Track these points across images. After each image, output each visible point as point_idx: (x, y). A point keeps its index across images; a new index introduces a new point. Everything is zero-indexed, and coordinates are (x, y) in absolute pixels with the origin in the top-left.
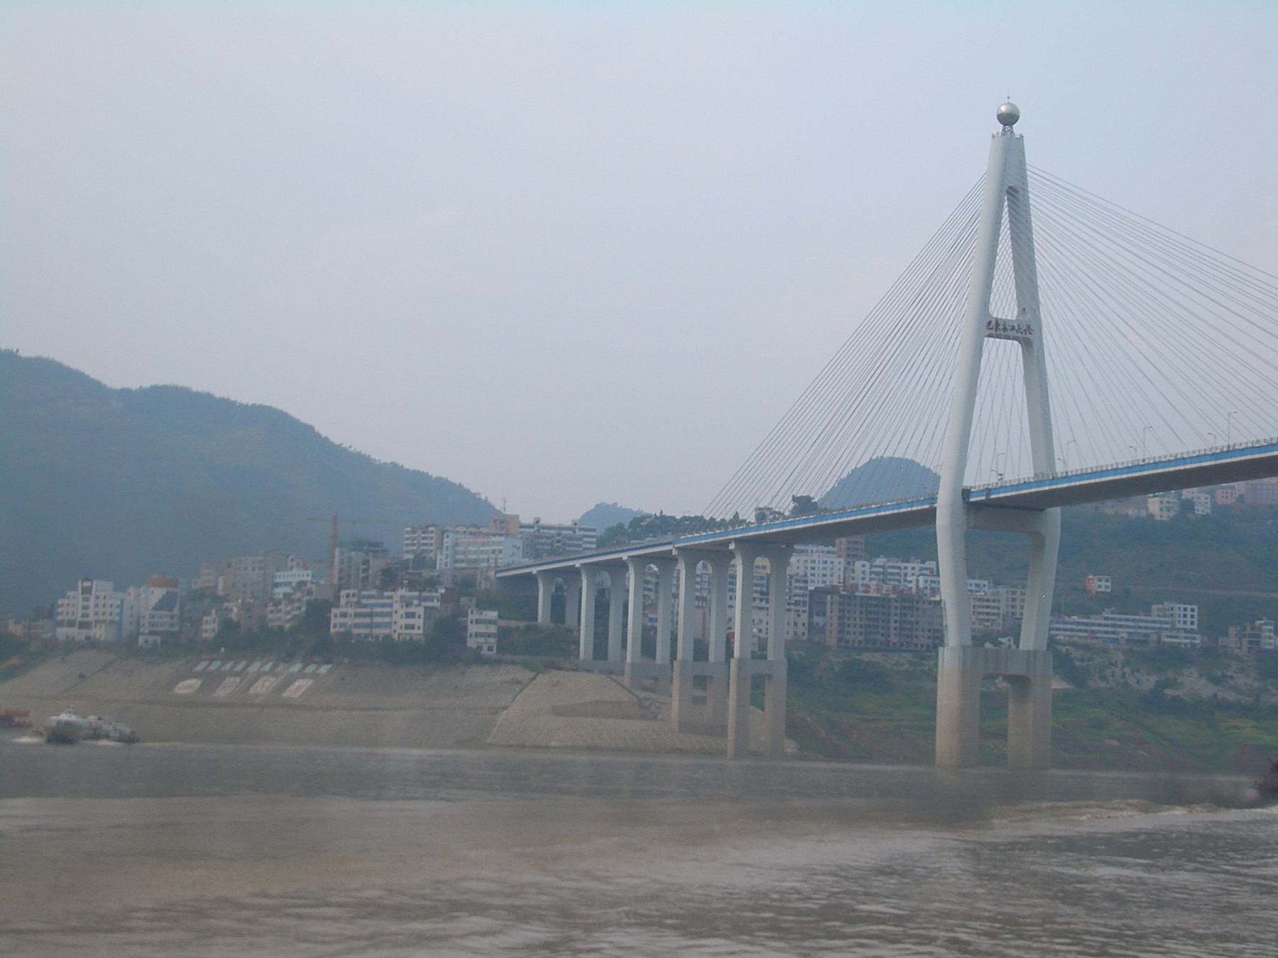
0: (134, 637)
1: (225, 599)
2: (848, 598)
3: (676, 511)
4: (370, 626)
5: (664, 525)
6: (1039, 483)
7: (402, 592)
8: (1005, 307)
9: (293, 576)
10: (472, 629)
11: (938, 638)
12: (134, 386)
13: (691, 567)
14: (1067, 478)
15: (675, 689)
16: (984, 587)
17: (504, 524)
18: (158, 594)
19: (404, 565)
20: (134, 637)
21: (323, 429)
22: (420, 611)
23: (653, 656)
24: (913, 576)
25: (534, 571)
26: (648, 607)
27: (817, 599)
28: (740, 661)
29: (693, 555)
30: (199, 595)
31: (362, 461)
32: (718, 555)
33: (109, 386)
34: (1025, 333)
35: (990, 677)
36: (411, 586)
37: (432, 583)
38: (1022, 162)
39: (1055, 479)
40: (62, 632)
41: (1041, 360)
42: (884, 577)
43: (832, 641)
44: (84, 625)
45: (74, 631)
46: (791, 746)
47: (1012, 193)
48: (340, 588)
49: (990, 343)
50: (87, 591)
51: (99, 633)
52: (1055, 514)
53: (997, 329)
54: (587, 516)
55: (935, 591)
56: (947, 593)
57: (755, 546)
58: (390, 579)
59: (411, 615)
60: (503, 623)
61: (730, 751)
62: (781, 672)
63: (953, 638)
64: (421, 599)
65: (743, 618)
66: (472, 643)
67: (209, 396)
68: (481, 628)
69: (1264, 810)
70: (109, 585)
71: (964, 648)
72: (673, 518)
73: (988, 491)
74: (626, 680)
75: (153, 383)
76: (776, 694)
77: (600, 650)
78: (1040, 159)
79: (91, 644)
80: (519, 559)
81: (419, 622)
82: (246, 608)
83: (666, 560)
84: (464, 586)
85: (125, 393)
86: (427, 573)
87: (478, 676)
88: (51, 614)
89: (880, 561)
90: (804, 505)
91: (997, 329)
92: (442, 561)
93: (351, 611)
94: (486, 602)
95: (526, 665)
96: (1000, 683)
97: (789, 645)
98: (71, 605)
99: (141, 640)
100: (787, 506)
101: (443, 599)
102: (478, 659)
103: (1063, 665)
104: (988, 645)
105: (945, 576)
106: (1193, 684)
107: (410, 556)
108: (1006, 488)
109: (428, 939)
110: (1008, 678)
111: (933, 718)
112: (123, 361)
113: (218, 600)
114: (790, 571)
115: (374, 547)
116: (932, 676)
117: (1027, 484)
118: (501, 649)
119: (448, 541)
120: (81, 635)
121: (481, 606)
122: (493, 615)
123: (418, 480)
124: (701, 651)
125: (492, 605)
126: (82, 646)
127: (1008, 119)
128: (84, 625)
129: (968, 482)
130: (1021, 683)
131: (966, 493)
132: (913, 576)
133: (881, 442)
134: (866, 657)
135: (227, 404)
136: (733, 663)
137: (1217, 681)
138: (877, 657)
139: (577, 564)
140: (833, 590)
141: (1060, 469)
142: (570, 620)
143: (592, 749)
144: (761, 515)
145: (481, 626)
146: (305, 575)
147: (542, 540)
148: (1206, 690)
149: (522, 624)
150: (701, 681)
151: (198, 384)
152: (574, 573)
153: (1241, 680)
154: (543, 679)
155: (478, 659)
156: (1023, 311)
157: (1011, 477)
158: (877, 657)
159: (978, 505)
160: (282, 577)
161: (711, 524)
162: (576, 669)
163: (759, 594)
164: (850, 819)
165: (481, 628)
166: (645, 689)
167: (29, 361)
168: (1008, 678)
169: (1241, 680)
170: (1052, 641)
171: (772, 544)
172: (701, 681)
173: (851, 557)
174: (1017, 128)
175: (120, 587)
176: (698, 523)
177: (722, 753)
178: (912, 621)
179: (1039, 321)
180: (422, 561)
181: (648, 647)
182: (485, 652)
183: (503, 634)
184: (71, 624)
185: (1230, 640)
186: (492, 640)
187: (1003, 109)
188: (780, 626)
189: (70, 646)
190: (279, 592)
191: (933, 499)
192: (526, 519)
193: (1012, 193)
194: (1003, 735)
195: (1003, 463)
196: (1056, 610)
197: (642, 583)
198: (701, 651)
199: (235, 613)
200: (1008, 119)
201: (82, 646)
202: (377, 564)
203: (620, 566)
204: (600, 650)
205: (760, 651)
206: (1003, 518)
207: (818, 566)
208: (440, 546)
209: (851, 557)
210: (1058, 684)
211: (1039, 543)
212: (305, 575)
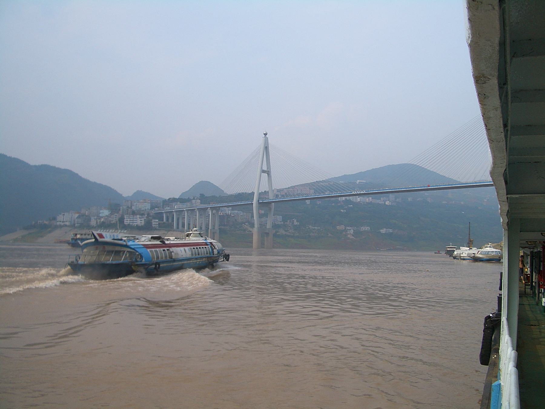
8: (265, 168)
10: (153, 223)
18: (77, 215)
21: (80, 174)
23: (184, 227)
33: (32, 163)
34: (268, 172)
40: (58, 223)
45: (61, 223)
47: (266, 148)
50: (63, 215)
51: (67, 223)
53: (264, 171)
75: (15, 157)
77: (178, 228)
78: (271, 142)
79: (66, 226)
85: (35, 166)
88: (54, 219)
91: (264, 171)
95: (166, 230)
98: (60, 218)
101: (147, 217)
106: (282, 232)
112: (34, 157)
118: (159, 227)
120: (62, 224)
127: (266, 134)
128: (63, 222)
133: (415, 256)
137: (286, 231)
145: (155, 223)
148: (284, 233)
153: (290, 231)
154: (169, 233)
156: (268, 168)
164: (41, 288)
169: (290, 231)
183: (159, 224)
185: (288, 223)
189: (61, 227)
193: (266, 148)
200: (266, 134)
204: (178, 228)
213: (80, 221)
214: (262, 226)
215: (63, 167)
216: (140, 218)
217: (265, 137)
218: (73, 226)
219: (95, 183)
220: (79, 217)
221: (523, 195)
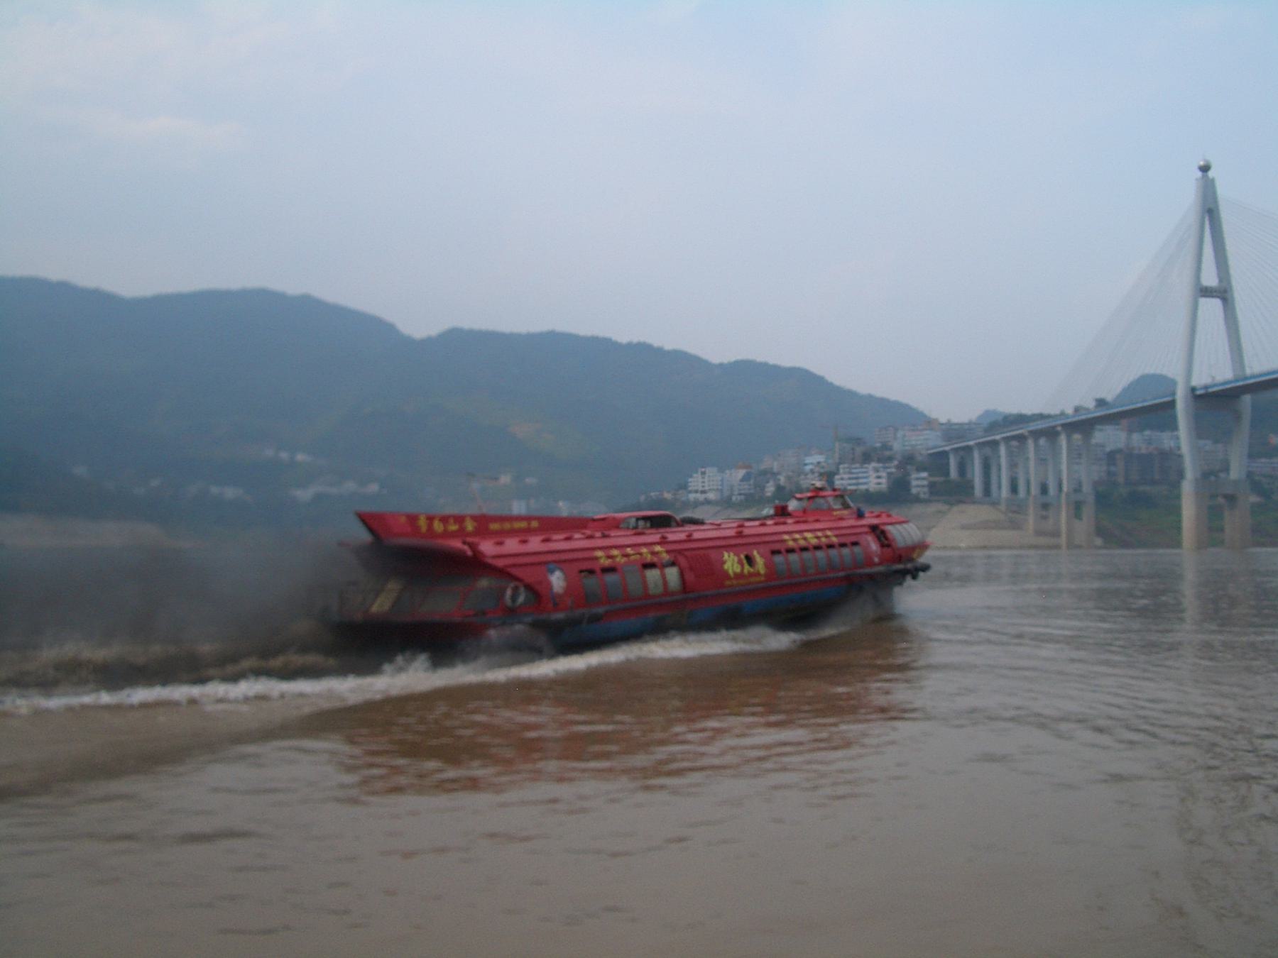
0: (730, 498)
1: (778, 473)
2: (1129, 455)
3: (1028, 410)
4: (857, 484)
5: (1021, 419)
6: (1237, 381)
7: (874, 465)
8: (1210, 278)
9: (814, 459)
10: (914, 483)
11: (1181, 474)
12: (725, 361)
13: (1036, 441)
14: (1253, 377)
15: (1031, 511)
16: (1208, 445)
17: (930, 423)
19: (875, 449)
20: (730, 498)
21: (837, 377)
22: (884, 474)
24: (1166, 440)
25: (947, 448)
26: (1013, 465)
27: (1111, 457)
28: (1068, 495)
29: (1037, 434)
30: (764, 473)
31: (851, 394)
32: (1051, 434)
34: (1223, 293)
35: (1213, 496)
36: (879, 461)
37: (890, 459)
38: (1214, 193)
39: (1246, 378)
40: (692, 496)
41: (1233, 309)
42: (1149, 442)
43: (1121, 480)
44: (703, 492)
45: (698, 495)
46: (1099, 541)
47: (1210, 211)
48: (840, 463)
49: (1202, 301)
50: (704, 473)
51: (711, 496)
52: (1247, 399)
53: (1206, 292)
54: (980, 417)
55: (1179, 448)
56: (1185, 449)
57: (1072, 427)
58: (867, 458)
59: (879, 477)
60: (933, 479)
61: (1063, 540)
62: (1091, 499)
63: (1190, 474)
64: (885, 468)
65: (1070, 470)
66: (914, 491)
67: (766, 364)
68: (919, 483)
69: (747, 647)
70: (715, 469)
71: (1196, 480)
72: (936, 420)
73: (1206, 387)
74: (1003, 507)
76: (1088, 511)
77: (987, 491)
78: (1222, 191)
79: (707, 502)
80: (940, 442)
81: (884, 481)
82: (788, 478)
83: (1021, 439)
84: (908, 460)
85: (721, 365)
86: (888, 453)
87: (918, 509)
88: (684, 486)
89: (1147, 433)
90: (1101, 403)
91: (1206, 292)
92: (897, 446)
93: (846, 476)
94: (921, 468)
96: (1221, 500)
97: (1096, 484)
98: (696, 482)
99: (734, 498)
100: (1091, 404)
101: (898, 467)
102: (917, 500)
103: (1256, 487)
104: (1213, 478)
105: (1183, 438)
107: (878, 445)
108: (1215, 385)
109: (240, 738)
110: (1226, 497)
111: (1180, 521)
113: (774, 474)
114: (1093, 441)
115: (858, 441)
116: (1178, 497)
117: (1230, 382)
118: (931, 493)
119: (900, 434)
120: (701, 497)
121: (919, 469)
122: (924, 474)
123: (883, 402)
124: (1044, 490)
125: (924, 469)
126: (702, 504)
127: (1205, 169)
128: (703, 492)
129: (1194, 383)
130: (1231, 499)
131: (1193, 389)
132: (1166, 440)
134: (1141, 488)
135: (776, 368)
136: (1063, 496)
138: (1147, 488)
139: (971, 443)
140: (1119, 451)
141: (1248, 372)
142: (969, 476)
143: (985, 547)
144: (1077, 410)
145: (919, 481)
146: (821, 458)
147: (952, 432)
149: (942, 479)
150: (1045, 506)
151: (666, 340)
152: (968, 449)
154: (955, 509)
155: (917, 500)
156: (1221, 281)
157: (1220, 378)
158: (1147, 488)
159: (1200, 396)
160: (808, 460)
161: (1049, 416)
162: (974, 503)
163: (1075, 455)
165: (919, 483)
166: (1014, 512)
167: (669, 352)
168: (1226, 497)
170: (1250, 475)
171: (1082, 426)
172: (1045, 506)
173: (1130, 431)
174: (1211, 174)
175: (721, 470)
176: (1041, 417)
177: (1057, 547)
178: (1164, 467)
179: (1231, 287)
180: (886, 447)
181: (1014, 489)
182: (922, 496)
183: (932, 486)
184: (696, 492)
186: (926, 490)
187: (1202, 163)
188: (1089, 474)
190: (808, 468)
191: (1174, 394)
192: (943, 420)
193: (1210, 211)
194: (1222, 530)
195: (1214, 369)
196: (1251, 456)
197: (1010, 454)
198: (1044, 490)
199: (782, 480)
200: (1205, 169)
201: (702, 504)
202: (859, 450)
203: (995, 444)
204: (987, 491)
205: (1078, 490)
206: (1216, 403)
207: (1110, 438)
208: (895, 438)
209: (1130, 431)
210: (1254, 499)
211: (1238, 417)
212: (821, 458)
213: (746, 487)
214: (1208, 476)
215: (786, 362)
216: (877, 470)
217: (1205, 177)
218: (726, 503)
219: (870, 397)
220: (745, 478)
221: (141, 695)
